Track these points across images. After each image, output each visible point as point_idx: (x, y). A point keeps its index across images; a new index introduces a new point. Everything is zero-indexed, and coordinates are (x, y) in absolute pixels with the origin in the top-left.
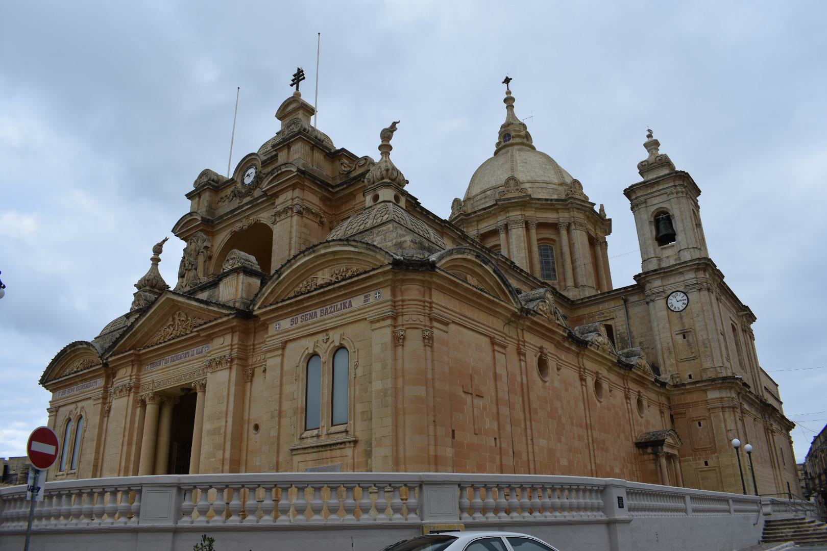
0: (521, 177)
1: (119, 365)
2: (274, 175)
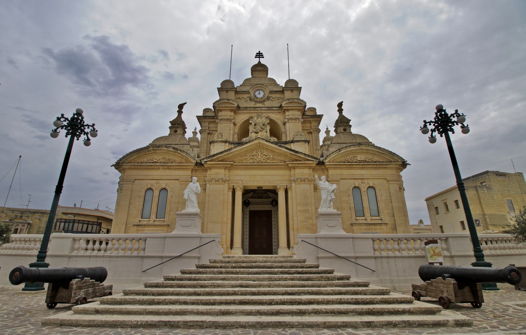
2: (289, 101)
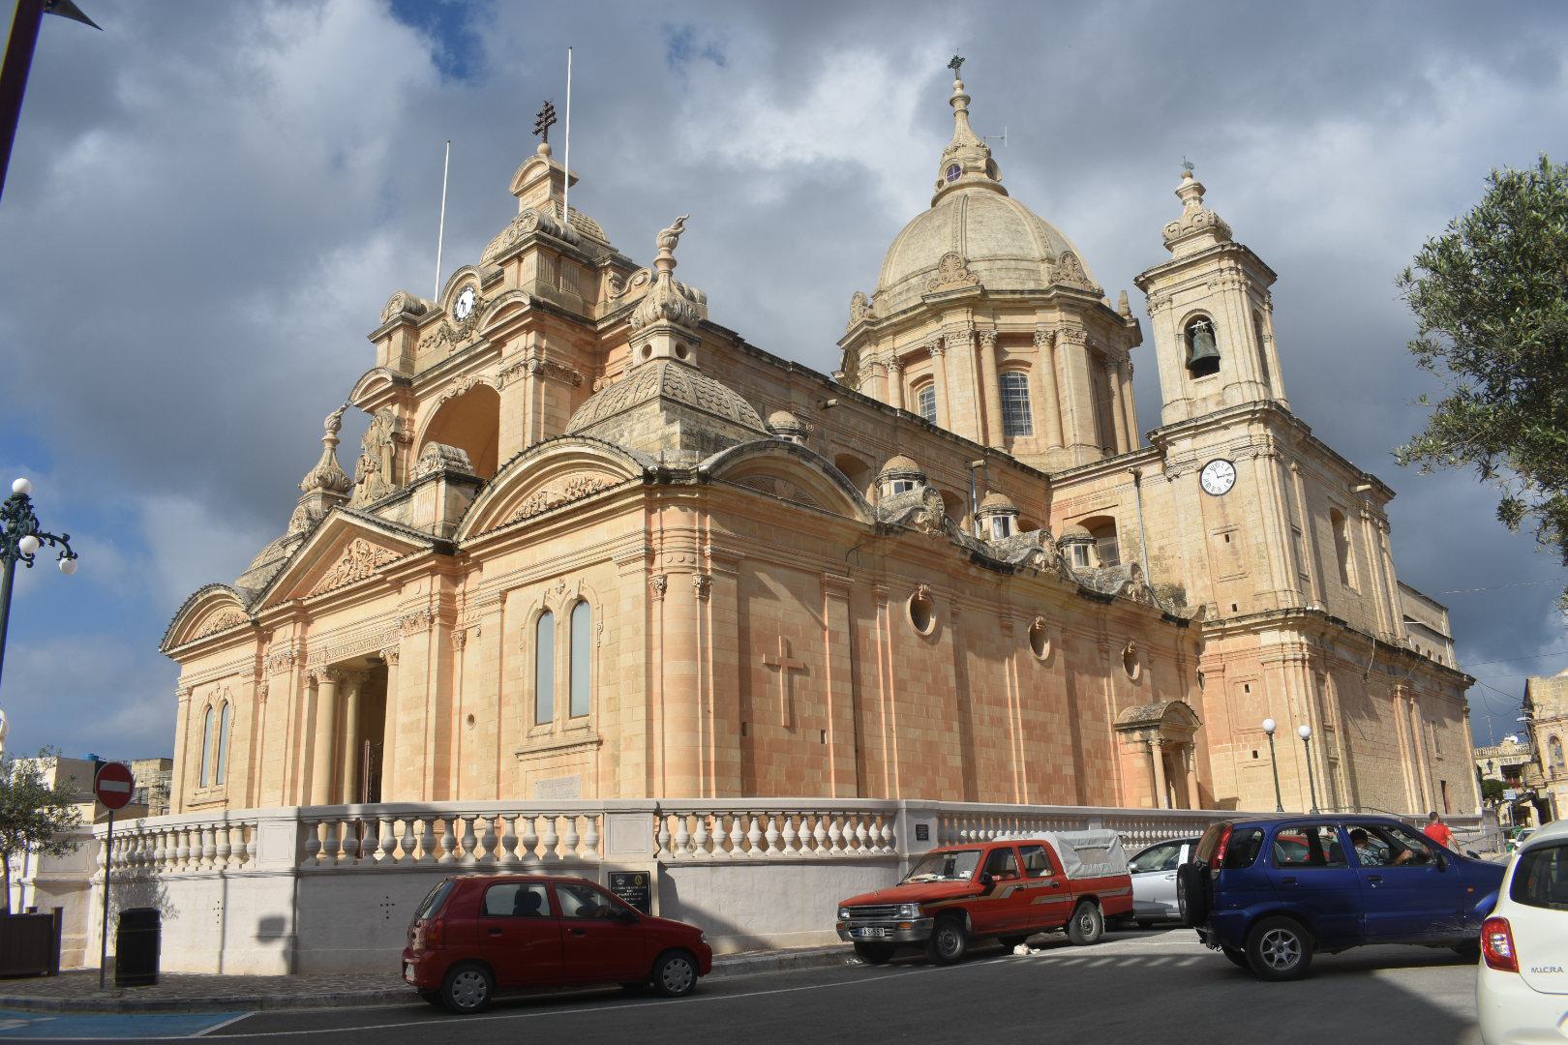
2: (497, 309)
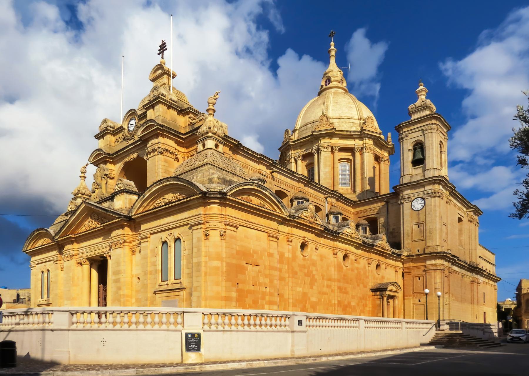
0: (330, 114)
1: (65, 243)
